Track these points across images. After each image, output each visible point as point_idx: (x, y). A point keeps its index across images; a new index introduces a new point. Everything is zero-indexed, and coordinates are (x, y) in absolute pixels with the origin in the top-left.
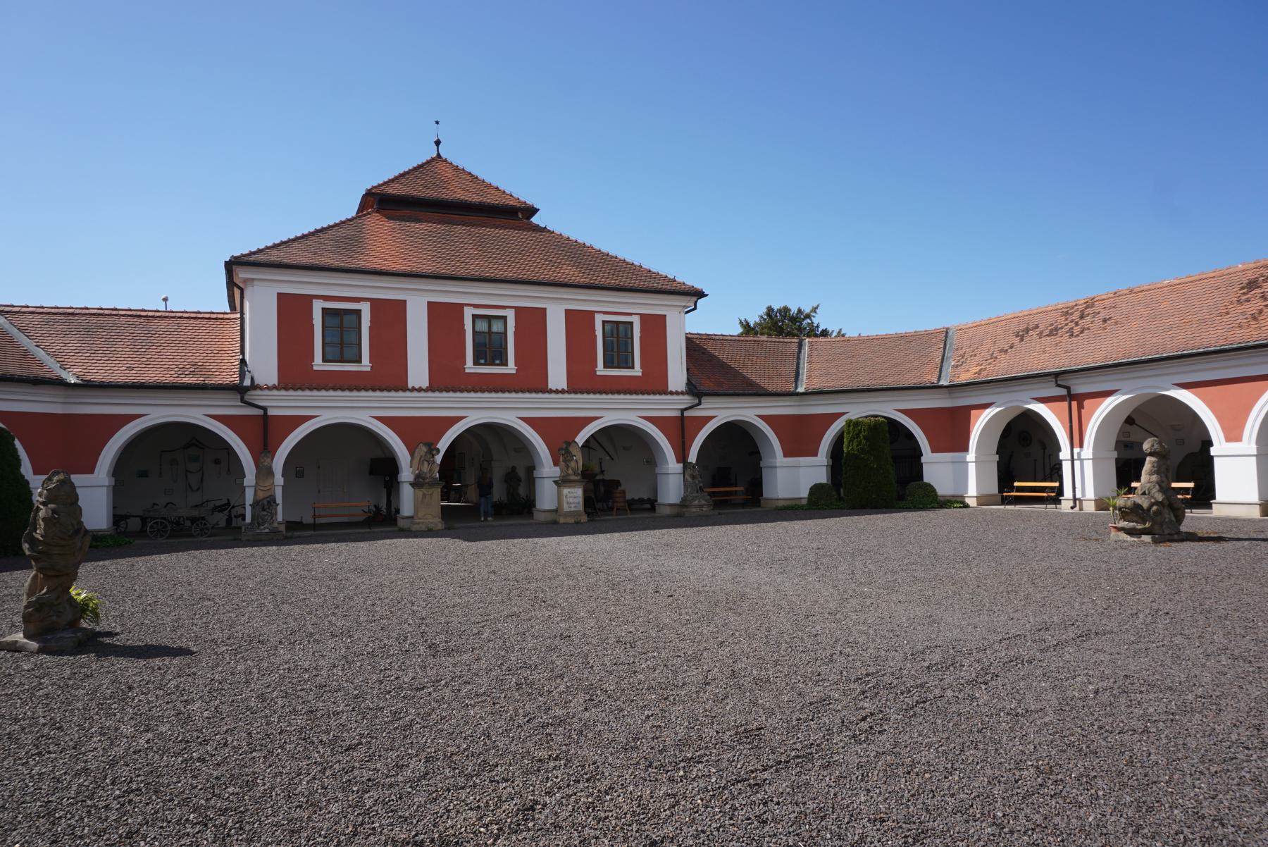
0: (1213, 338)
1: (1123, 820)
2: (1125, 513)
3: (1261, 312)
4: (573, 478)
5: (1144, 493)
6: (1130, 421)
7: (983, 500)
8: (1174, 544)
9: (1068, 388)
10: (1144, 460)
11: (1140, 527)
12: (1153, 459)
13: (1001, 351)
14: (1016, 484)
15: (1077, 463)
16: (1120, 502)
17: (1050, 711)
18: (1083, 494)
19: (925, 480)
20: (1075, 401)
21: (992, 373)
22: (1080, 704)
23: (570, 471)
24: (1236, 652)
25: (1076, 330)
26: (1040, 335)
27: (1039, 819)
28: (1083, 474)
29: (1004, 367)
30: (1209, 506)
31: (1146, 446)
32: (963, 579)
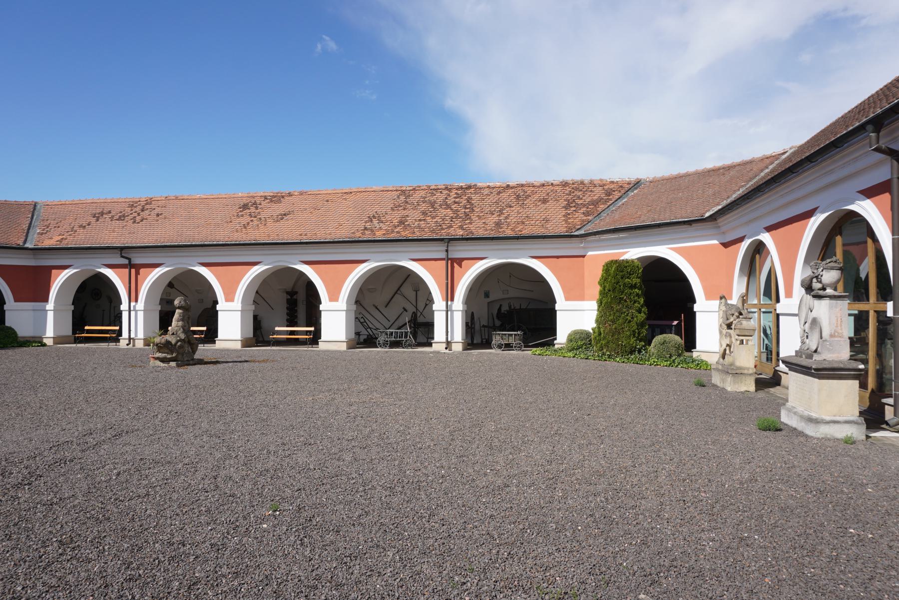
0: (222, 236)
1: (119, 562)
2: (160, 347)
3: (248, 224)
5: (173, 334)
6: (170, 285)
7: (58, 340)
8: (189, 367)
9: (130, 259)
10: (174, 312)
11: (169, 356)
12: (181, 311)
13: (81, 226)
14: (86, 328)
15: (133, 313)
16: (157, 340)
17: (80, 495)
18: (136, 335)
19: (7, 324)
20: (134, 269)
21: (71, 242)
22: (105, 484)
24: (213, 433)
25: (138, 219)
26: (112, 218)
27: (54, 581)
28: (137, 321)
29: (81, 239)
30: (214, 342)
31: (176, 302)
32: (28, 404)
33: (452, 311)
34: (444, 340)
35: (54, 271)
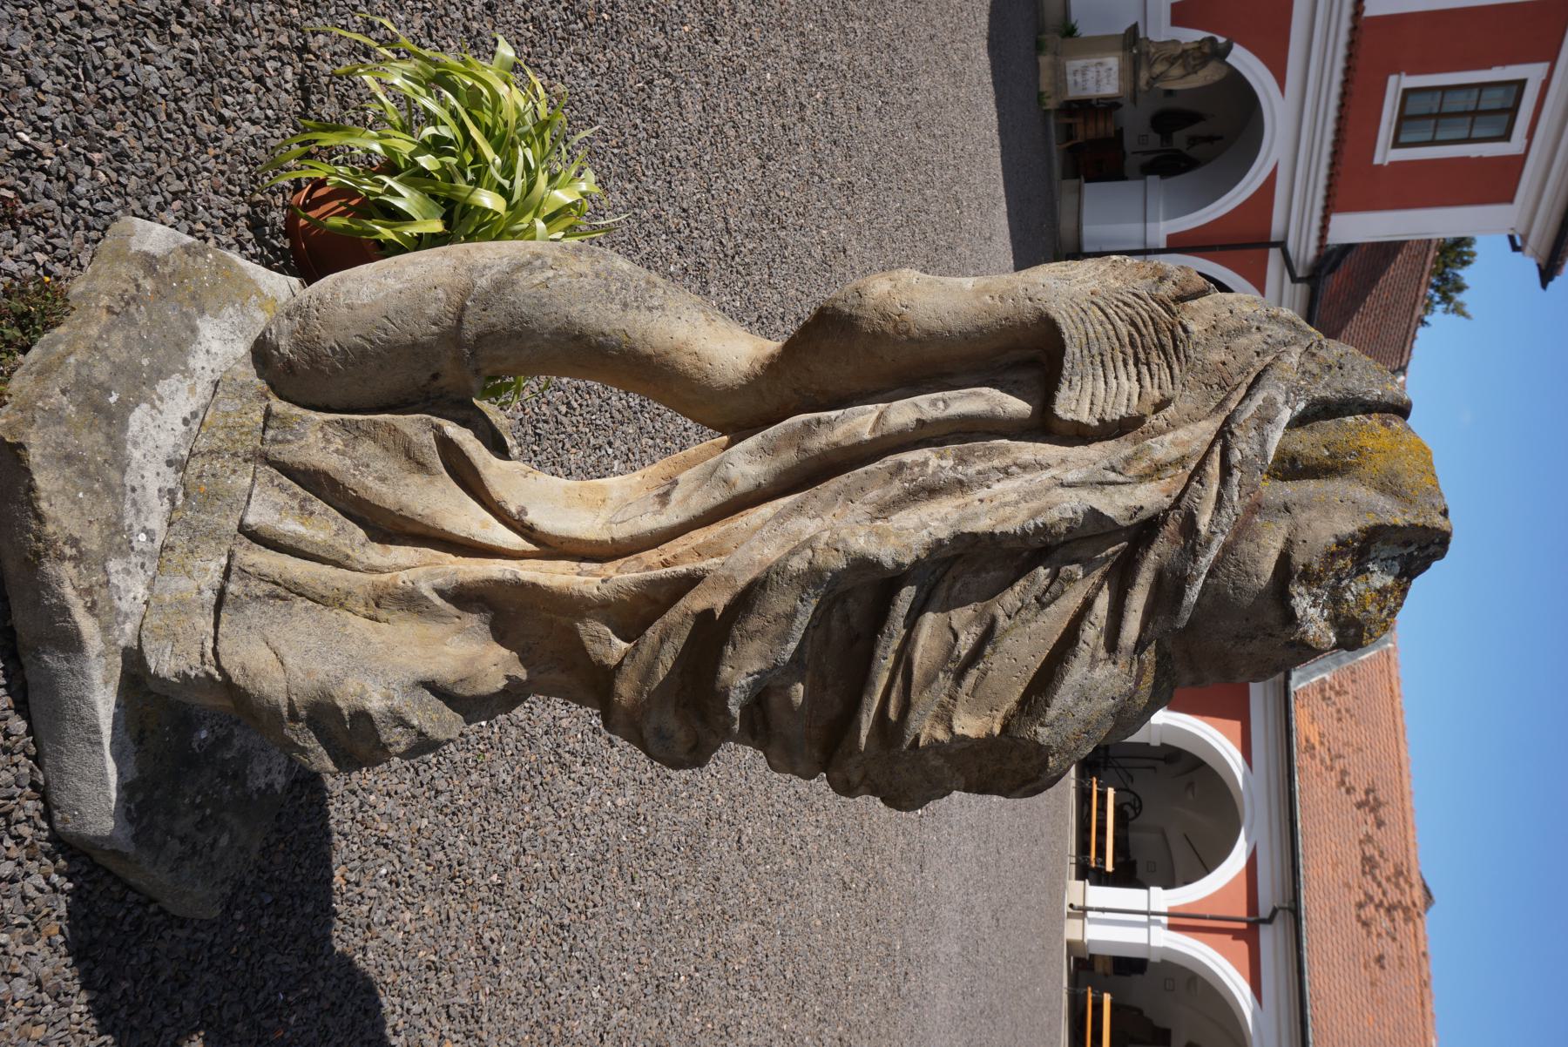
4: (1144, 76)
9: (1269, 921)
13: (1344, 773)
14: (1111, 792)
15: (1144, 918)
23: (1159, 68)
33: (1148, 925)
34: (1089, 904)
35: (1236, 726)
